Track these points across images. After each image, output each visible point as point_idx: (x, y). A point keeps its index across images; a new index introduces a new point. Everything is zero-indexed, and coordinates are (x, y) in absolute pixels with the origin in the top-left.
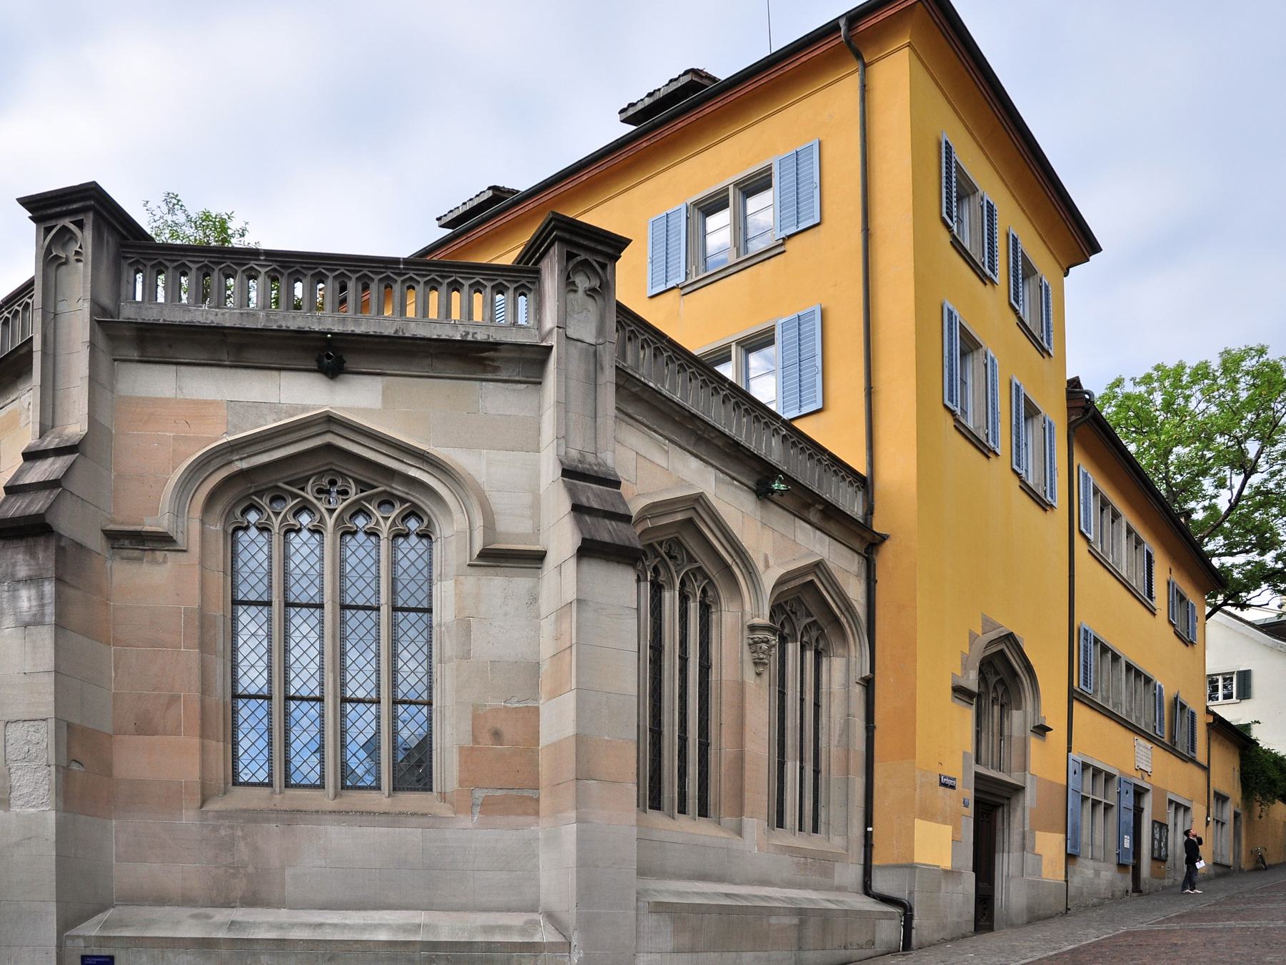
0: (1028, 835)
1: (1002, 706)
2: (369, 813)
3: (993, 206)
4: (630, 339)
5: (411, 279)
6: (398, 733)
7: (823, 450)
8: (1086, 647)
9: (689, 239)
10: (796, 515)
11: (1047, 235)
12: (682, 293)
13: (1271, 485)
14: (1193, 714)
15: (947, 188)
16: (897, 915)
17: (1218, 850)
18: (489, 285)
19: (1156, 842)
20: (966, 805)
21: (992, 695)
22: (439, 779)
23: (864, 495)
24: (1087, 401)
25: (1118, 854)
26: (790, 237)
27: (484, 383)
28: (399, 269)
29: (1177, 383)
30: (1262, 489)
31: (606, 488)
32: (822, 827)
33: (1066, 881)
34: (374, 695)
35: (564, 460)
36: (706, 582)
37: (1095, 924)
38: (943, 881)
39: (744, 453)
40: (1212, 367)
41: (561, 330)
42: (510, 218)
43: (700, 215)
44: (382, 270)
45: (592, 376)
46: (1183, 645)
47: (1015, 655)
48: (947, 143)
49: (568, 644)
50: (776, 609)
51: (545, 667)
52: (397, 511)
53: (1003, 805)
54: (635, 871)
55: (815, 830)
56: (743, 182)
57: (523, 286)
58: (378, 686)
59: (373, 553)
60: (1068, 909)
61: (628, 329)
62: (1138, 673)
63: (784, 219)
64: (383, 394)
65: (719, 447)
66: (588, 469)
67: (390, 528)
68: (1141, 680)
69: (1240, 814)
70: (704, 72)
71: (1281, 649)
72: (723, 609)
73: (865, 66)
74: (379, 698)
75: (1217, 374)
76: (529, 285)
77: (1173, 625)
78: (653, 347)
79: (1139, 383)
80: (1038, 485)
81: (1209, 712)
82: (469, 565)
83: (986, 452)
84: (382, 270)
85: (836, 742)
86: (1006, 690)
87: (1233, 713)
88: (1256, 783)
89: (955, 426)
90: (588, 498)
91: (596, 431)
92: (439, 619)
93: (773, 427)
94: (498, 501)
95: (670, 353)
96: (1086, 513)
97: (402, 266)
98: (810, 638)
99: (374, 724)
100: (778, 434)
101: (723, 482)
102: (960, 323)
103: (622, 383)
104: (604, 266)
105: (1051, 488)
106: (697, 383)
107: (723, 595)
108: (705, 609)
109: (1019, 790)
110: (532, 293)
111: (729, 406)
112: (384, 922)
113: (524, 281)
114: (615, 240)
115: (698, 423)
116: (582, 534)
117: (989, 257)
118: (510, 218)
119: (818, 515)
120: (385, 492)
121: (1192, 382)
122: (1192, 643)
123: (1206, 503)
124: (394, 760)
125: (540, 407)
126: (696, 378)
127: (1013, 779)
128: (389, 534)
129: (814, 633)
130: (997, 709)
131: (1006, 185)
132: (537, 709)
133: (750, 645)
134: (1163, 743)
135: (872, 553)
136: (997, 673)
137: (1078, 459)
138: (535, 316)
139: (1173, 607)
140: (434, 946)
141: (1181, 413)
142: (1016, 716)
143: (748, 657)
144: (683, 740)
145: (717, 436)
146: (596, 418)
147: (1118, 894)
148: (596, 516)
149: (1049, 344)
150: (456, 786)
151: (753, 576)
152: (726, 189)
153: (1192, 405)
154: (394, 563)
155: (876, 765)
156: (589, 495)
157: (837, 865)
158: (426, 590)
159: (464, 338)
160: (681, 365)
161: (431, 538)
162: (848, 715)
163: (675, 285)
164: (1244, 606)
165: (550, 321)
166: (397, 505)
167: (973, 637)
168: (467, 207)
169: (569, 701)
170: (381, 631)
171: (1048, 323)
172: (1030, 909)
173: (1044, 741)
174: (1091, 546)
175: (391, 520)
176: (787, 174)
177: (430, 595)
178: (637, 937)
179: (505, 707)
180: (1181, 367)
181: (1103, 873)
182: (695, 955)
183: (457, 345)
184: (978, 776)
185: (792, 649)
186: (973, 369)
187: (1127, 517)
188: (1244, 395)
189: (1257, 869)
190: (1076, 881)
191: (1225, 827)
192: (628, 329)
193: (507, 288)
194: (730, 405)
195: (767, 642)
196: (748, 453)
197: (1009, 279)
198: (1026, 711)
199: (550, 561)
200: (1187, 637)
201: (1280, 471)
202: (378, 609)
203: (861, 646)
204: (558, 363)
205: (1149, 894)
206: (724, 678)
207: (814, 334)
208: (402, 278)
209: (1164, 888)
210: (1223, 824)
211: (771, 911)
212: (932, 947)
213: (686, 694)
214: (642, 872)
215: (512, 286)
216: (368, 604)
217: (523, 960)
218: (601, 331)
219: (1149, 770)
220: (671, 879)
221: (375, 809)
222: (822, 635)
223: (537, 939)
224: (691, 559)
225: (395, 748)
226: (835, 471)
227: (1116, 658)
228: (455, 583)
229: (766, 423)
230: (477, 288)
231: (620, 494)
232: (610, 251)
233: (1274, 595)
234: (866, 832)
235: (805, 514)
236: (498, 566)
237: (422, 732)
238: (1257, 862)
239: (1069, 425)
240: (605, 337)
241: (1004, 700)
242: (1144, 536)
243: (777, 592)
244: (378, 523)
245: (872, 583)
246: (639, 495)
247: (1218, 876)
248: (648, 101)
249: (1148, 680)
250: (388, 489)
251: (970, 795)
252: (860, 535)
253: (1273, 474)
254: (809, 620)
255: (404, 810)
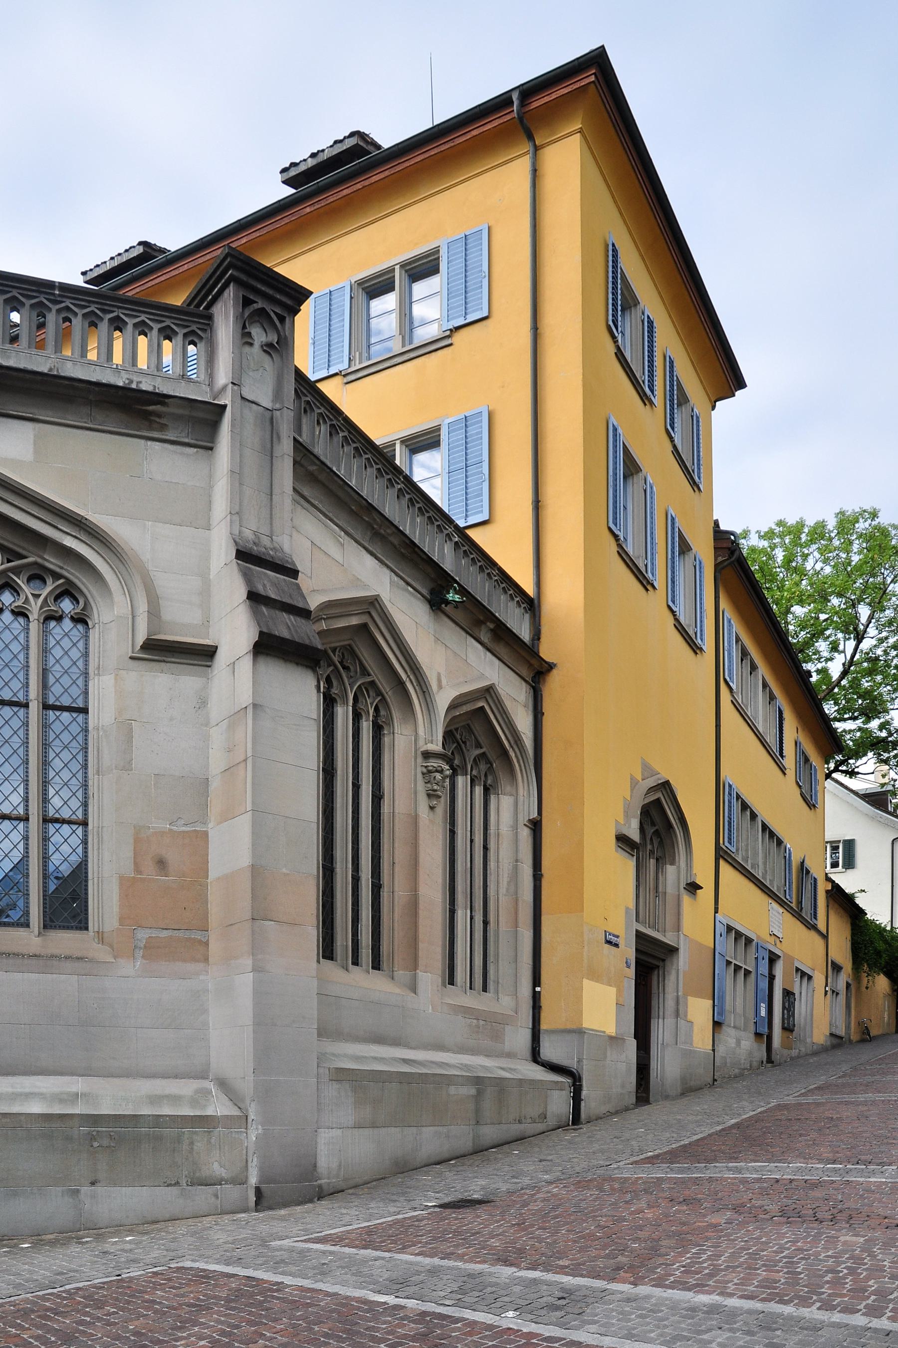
0: (681, 1000)
1: (657, 860)
2: (16, 955)
3: (652, 322)
4: (305, 411)
5: (68, 309)
6: (49, 858)
7: (493, 564)
8: (730, 802)
9: (353, 318)
10: (467, 633)
11: (699, 363)
12: (345, 381)
13: (879, 652)
14: (815, 879)
15: (613, 294)
16: (567, 1085)
17: (833, 1021)
18: (156, 327)
19: (786, 1011)
20: (628, 966)
21: (649, 847)
22: (96, 914)
23: (531, 618)
24: (733, 542)
25: (756, 1023)
26: (458, 328)
27: (149, 443)
28: (54, 294)
29: (796, 542)
30: (870, 655)
31: (282, 577)
32: (491, 986)
33: (714, 1050)
34: (21, 810)
35: (237, 540)
36: (379, 698)
37: (746, 1097)
38: (608, 1047)
39: (418, 555)
40: (828, 527)
41: (236, 388)
42: (162, 278)
43: (365, 296)
44: (34, 294)
45: (269, 446)
46: (808, 808)
47: (672, 808)
48: (613, 245)
49: (242, 758)
50: (449, 735)
51: (215, 784)
52: (49, 588)
53: (658, 967)
54: (315, 1031)
55: (485, 989)
56: (410, 263)
57: (193, 333)
58: (26, 800)
59: (21, 638)
60: (715, 1080)
61: (304, 399)
62: (772, 834)
63: (452, 308)
64: (35, 444)
65: (395, 547)
66: (264, 554)
67: (41, 608)
68: (773, 842)
69: (850, 985)
70: (369, 137)
71: (880, 819)
72: (396, 731)
73: (536, 149)
74: (27, 814)
75: (833, 535)
76: (199, 332)
77: (800, 787)
78: (329, 423)
79: (763, 537)
80: (689, 626)
81: (828, 879)
82: (131, 658)
83: (645, 583)
84: (34, 294)
85: (505, 890)
86: (661, 843)
87: (847, 881)
88: (865, 954)
89: (618, 551)
90: (264, 586)
91: (271, 510)
92: (96, 721)
93: (446, 532)
94: (165, 583)
95: (346, 434)
96: (730, 662)
97: (57, 292)
98: (479, 772)
99: (21, 846)
100: (451, 540)
101: (398, 587)
102: (623, 443)
103: (298, 459)
104: (282, 319)
105: (701, 631)
106: (372, 472)
107: (396, 715)
108: (378, 730)
109: (672, 951)
110: (204, 341)
111: (403, 502)
112: (36, 1090)
113: (194, 327)
114: (296, 291)
115: (375, 515)
116: (260, 627)
117: (649, 376)
118: (162, 278)
119: (489, 635)
120: (36, 563)
121: (811, 540)
122: (814, 806)
123: (820, 666)
124: (44, 891)
125: (210, 476)
126: (372, 466)
127: (668, 939)
128: (40, 615)
129: (483, 767)
130: (653, 862)
131: (664, 304)
132: (206, 834)
133: (423, 774)
134: (792, 908)
135: (539, 683)
136: (653, 824)
137: (724, 604)
138: (207, 370)
139: (800, 768)
140: (95, 1120)
141: (800, 572)
142: (670, 870)
143: (421, 787)
144: (356, 879)
145: (394, 532)
146: (271, 495)
147: (755, 1064)
148: (274, 608)
149: (699, 478)
150: (116, 924)
151: (427, 696)
152: (391, 270)
153: (809, 565)
154: (45, 651)
155: (543, 918)
156: (266, 582)
157: (508, 1028)
158: (81, 686)
159: (128, 386)
160: (356, 449)
161: (87, 624)
162: (517, 861)
163: (337, 371)
164: (852, 774)
165: (223, 377)
166: (49, 581)
167: (634, 783)
168: (116, 263)
169: (243, 825)
170: (30, 733)
171: (698, 456)
172: (684, 1079)
173: (695, 899)
174: (733, 696)
175: (42, 598)
176: (456, 259)
177: (86, 693)
178: (319, 1110)
179: (170, 830)
180: (801, 525)
181: (743, 1042)
182: (376, 1131)
183: (120, 393)
184: (639, 935)
185: (462, 782)
186: (633, 491)
187: (763, 670)
188: (855, 559)
189: (862, 1041)
190: (721, 1050)
191: (839, 997)
192: (304, 399)
193: (176, 333)
194: (405, 501)
195: (441, 771)
196: (425, 557)
197: (665, 404)
198: (679, 867)
199: (222, 658)
200: (811, 801)
201: (887, 638)
202: (26, 706)
203: (528, 783)
204: (233, 425)
205: (780, 1065)
206: (396, 811)
207: (481, 438)
208: (58, 307)
209: (792, 1058)
210: (837, 994)
211: (449, 1080)
212: (600, 1121)
213: (358, 827)
214: (322, 1033)
215: (181, 332)
216: (15, 699)
217: (195, 1137)
218: (278, 395)
219: (780, 936)
220: (347, 1041)
221: (25, 951)
222: (491, 769)
223: (209, 1112)
224: (365, 672)
225: (45, 876)
226: (504, 588)
227: (754, 816)
228: (116, 679)
229: (438, 526)
230: (142, 329)
231: (298, 586)
232: (289, 302)
233: (878, 764)
234: (534, 992)
235: (476, 632)
236: (164, 661)
237: (75, 859)
238: (863, 1033)
239: (716, 566)
240: (282, 402)
241: (659, 854)
242: (777, 692)
243: (450, 717)
244: (27, 600)
245: (539, 716)
246: (314, 591)
247: (834, 1047)
248: (311, 163)
249: (780, 842)
250: (39, 560)
251: (631, 953)
252: (529, 662)
253: (881, 641)
254: (479, 752)
255: (56, 951)
